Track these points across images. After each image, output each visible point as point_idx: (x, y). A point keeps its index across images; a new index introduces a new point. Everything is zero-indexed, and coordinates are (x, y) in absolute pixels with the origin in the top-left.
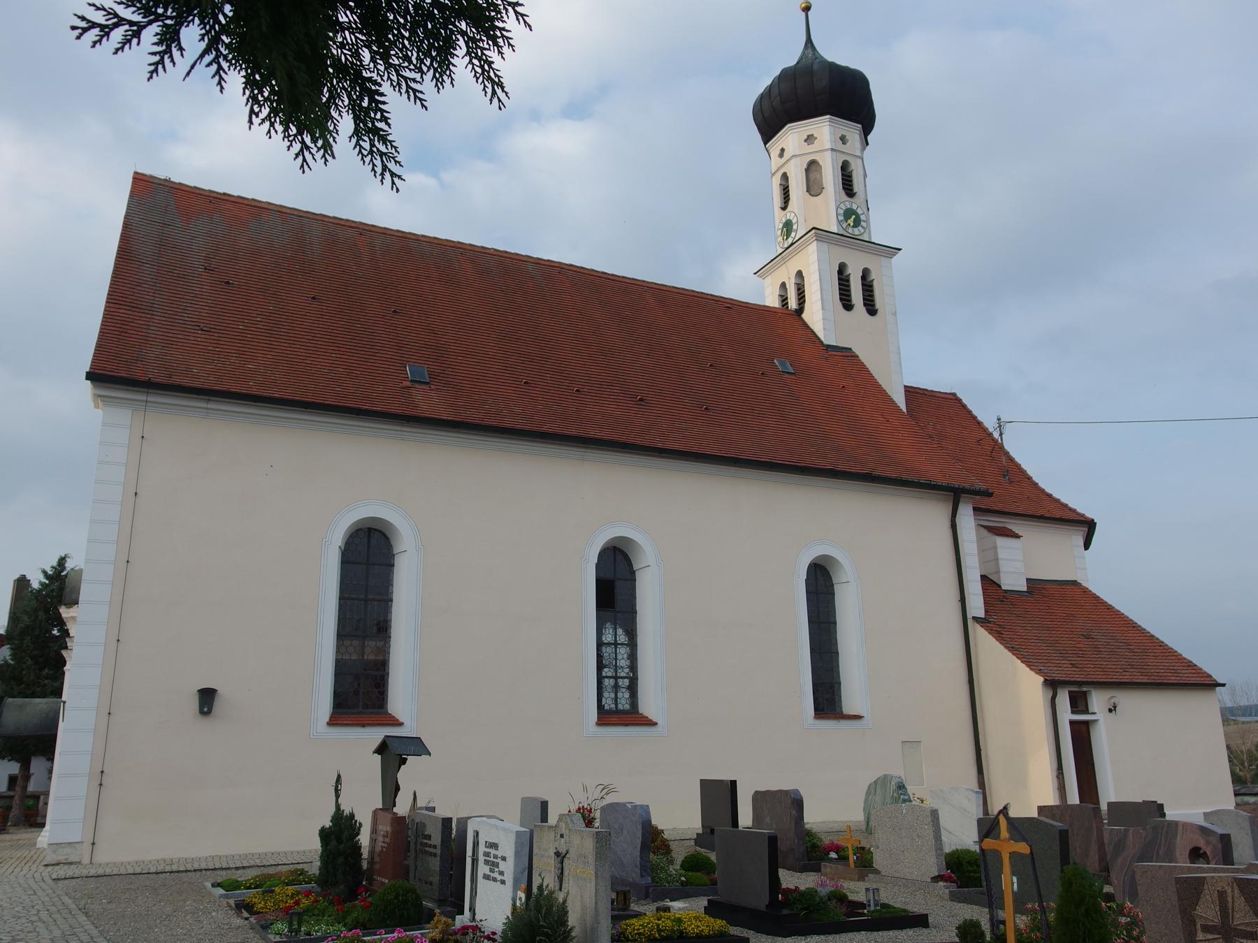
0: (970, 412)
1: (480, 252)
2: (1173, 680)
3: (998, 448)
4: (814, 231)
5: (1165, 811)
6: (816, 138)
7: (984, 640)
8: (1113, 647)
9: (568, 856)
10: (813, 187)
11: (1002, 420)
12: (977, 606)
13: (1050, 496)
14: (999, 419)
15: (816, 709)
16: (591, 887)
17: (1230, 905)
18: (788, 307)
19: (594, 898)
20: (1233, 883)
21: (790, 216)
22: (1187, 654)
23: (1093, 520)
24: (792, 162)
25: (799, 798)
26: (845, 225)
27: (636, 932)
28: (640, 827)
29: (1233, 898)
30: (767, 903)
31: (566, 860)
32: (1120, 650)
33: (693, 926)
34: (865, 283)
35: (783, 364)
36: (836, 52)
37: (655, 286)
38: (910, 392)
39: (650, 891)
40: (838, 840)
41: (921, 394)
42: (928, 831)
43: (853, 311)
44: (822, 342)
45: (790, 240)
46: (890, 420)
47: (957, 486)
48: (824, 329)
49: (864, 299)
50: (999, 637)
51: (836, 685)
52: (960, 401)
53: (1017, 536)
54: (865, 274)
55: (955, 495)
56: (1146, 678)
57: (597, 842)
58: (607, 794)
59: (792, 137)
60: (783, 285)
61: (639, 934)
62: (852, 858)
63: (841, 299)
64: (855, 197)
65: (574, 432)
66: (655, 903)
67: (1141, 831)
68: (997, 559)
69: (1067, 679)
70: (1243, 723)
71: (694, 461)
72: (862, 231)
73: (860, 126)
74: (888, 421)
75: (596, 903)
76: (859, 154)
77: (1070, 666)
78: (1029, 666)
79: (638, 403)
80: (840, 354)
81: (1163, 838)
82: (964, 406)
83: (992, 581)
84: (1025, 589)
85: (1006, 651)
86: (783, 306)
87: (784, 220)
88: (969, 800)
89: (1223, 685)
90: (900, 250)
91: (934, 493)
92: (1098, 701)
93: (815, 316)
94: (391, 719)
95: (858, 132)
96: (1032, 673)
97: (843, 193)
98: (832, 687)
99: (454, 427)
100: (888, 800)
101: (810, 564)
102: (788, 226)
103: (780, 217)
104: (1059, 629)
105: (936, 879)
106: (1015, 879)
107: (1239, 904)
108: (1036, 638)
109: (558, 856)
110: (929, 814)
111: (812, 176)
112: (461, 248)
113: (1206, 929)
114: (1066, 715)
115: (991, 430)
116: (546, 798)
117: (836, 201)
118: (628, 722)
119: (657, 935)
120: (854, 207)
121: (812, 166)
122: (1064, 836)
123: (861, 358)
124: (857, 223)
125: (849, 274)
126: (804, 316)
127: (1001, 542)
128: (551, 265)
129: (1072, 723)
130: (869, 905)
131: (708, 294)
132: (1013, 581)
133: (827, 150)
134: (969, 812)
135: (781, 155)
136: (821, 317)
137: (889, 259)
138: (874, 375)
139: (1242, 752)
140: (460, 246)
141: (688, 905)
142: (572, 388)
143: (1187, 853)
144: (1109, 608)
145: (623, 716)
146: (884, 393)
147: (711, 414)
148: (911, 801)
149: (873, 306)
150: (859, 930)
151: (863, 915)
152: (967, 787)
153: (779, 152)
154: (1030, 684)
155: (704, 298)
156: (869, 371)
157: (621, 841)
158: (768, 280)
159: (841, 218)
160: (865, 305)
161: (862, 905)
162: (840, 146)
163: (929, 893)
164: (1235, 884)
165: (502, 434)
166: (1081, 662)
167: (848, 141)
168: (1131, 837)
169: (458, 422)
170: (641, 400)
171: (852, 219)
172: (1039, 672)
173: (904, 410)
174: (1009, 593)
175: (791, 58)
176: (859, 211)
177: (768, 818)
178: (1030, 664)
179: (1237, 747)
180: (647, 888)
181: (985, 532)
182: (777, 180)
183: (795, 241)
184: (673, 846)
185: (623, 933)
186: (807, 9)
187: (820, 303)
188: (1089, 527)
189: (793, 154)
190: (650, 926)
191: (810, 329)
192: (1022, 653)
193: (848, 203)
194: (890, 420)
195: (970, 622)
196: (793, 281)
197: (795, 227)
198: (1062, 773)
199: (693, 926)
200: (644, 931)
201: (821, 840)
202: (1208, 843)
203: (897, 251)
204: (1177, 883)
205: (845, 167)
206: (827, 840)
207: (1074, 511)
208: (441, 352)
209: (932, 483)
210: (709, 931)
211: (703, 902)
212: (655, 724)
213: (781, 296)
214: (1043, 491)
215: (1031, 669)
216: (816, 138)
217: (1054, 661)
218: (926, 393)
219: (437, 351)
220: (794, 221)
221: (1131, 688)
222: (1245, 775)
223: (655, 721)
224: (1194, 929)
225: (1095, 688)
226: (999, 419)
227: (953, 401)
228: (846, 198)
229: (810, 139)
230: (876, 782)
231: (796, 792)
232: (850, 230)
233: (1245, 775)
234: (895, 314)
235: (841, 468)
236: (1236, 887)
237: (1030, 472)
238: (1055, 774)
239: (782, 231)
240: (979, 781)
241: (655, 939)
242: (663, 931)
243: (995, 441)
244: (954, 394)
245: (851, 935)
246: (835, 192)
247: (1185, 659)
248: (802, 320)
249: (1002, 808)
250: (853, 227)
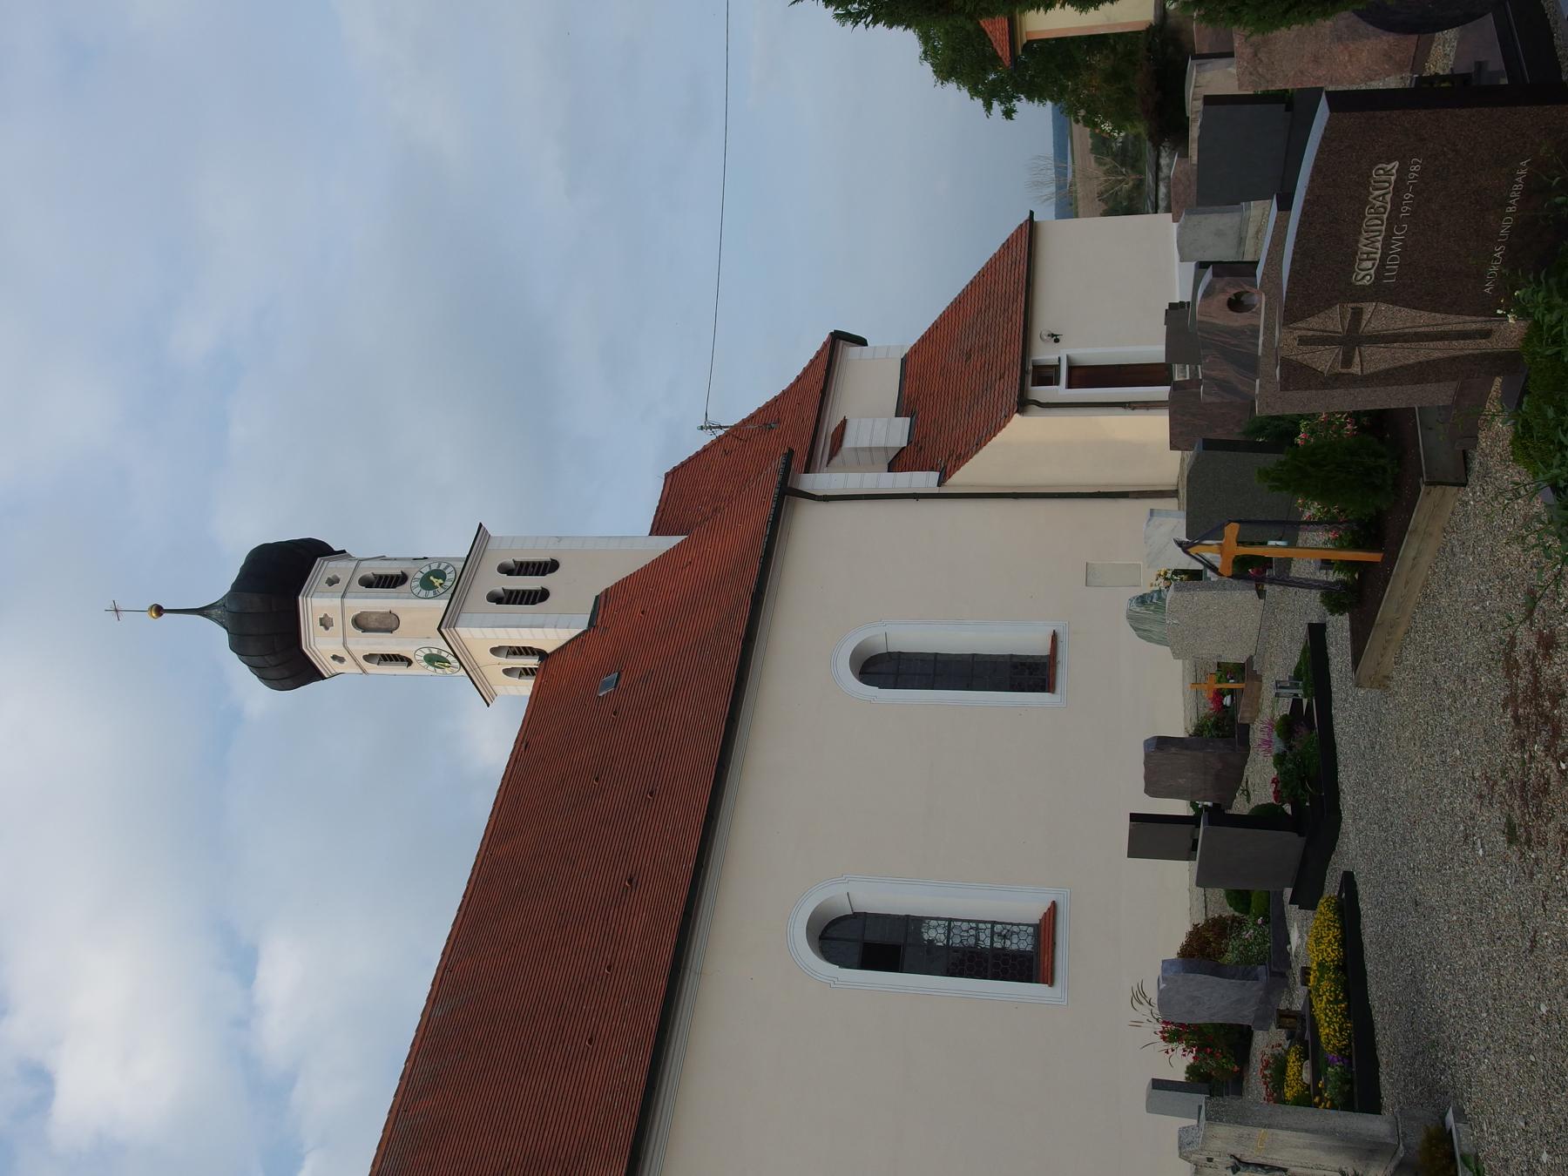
0: (690, 459)
1: (408, 1083)
2: (1023, 268)
3: (736, 432)
4: (443, 630)
5: (1178, 302)
6: (326, 615)
7: (966, 476)
8: (982, 329)
9: (1238, 1156)
10: (388, 624)
11: (703, 425)
12: (925, 480)
13: (799, 379)
14: (702, 428)
15: (1043, 690)
16: (1283, 1135)
17: (1318, 334)
18: (536, 669)
19: (1299, 1133)
20: (1289, 328)
21: (421, 655)
22: (995, 248)
23: (831, 334)
24: (351, 647)
25: (1155, 741)
26: (441, 590)
27: (1338, 1034)
28: (1191, 976)
29: (1309, 330)
30: (1296, 835)
31: (1245, 1159)
32: (986, 321)
33: (1329, 949)
34: (505, 599)
35: (606, 685)
36: (220, 581)
37: (487, 841)
38: (658, 528)
39: (1276, 970)
40: (1207, 695)
41: (662, 515)
43: (560, 562)
44: (584, 632)
45: (451, 659)
47: (777, 490)
48: (568, 628)
49: (537, 575)
50: (963, 458)
51: (1015, 660)
52: (675, 470)
53: (844, 422)
54: (506, 570)
55: (788, 494)
56: (1020, 296)
57: (1221, 1121)
58: (1145, 997)
59: (319, 644)
60: (507, 672)
61: (1341, 1030)
62: (1232, 684)
64: (407, 574)
65: (663, 983)
66: (1293, 965)
67: (1207, 361)
68: (870, 449)
69: (1017, 387)
70: (1074, 176)
71: (717, 822)
72: (451, 569)
73: (319, 559)
74: (690, 563)
75: (1307, 1131)
76: (353, 564)
77: (1002, 380)
78: (1000, 429)
79: (634, 886)
80: (601, 611)
81: (1216, 339)
82: (683, 465)
83: (895, 457)
84: (908, 419)
85: (981, 452)
86: (533, 674)
87: (425, 664)
88: (1161, 525)
89: (1032, 213)
90: (481, 525)
91: (783, 524)
92: (1044, 353)
93: (550, 638)
94: (1047, 918)
96: (1008, 425)
97: (399, 588)
98: (1015, 666)
100: (1158, 617)
101: (861, 680)
102: (432, 659)
103: (420, 669)
104: (958, 388)
105: (1261, 594)
106: (1271, 543)
107: (1315, 324)
108: (967, 415)
109: (1238, 1170)
110: (1180, 594)
111: (373, 625)
112: (398, 1111)
113: (1347, 362)
114: (1060, 392)
115: (714, 438)
116: (1148, 1081)
118: (1050, 943)
119: (1343, 1005)
120: (420, 576)
121: (360, 623)
122: (1209, 445)
124: (440, 574)
125: (503, 589)
126: (549, 650)
127: (849, 442)
128: (438, 983)
129: (1070, 386)
130: (1296, 695)
131: (506, 771)
132: (897, 433)
134: (1175, 527)
135: (341, 660)
136: (553, 630)
137: (491, 541)
138: (639, 568)
139: (1106, 181)
140: (395, 1112)
141: (1295, 924)
142: (605, 975)
143: (1235, 314)
144: (936, 327)
145: (1042, 946)
146: (655, 563)
147: (658, 788)
148: (1160, 591)
149: (546, 563)
150: (1330, 717)
151: (1309, 706)
152: (1144, 526)
153: (336, 662)
154: (1021, 429)
155: (511, 776)
157: (1209, 1000)
158: (499, 690)
159: (431, 593)
160: (543, 574)
161: (1296, 703)
162: (340, 587)
163: (1278, 604)
164: (1291, 325)
166: (998, 368)
167: (335, 576)
168: (1212, 373)
169: (632, 1152)
170: (630, 881)
171: (435, 580)
172: (1008, 418)
173: (683, 537)
174: (911, 439)
175: (221, 636)
176: (426, 570)
177: (1180, 780)
178: (998, 425)
179: (1101, 184)
180: (1273, 974)
181: (836, 460)
182: (372, 668)
183: (450, 651)
184: (1214, 913)
185: (1340, 1051)
186: (159, 610)
187: (534, 630)
188: (839, 339)
190: (1330, 1013)
191: (566, 644)
192: (984, 435)
193: (414, 584)
194: (690, 560)
195: (943, 490)
196: (503, 660)
197: (435, 651)
198: (1129, 403)
199: (1329, 949)
200: (1337, 1022)
201: (1207, 717)
202: (1223, 291)
203: (482, 528)
204: (1287, 389)
205: (367, 583)
206: (1208, 708)
207: (819, 354)
208: (534, 1162)
209: (771, 519)
210: (1335, 927)
211: (1293, 912)
212: (1054, 903)
213: (520, 676)
214: (792, 386)
215: (1004, 426)
216: (326, 615)
217: (996, 399)
218: (662, 508)
219: (532, 1168)
220: (428, 652)
221: (1032, 313)
222: (1133, 180)
223: (1050, 904)
224: (1347, 376)
225: (1029, 356)
226: (702, 428)
227: (673, 477)
229: (325, 623)
230: (1136, 629)
231: (1147, 743)
232: (448, 584)
233: (1133, 180)
234: (560, 539)
235: (742, 631)
236: (1295, 325)
237: (769, 398)
238: (1129, 411)
239: (438, 667)
240: (1137, 498)
241: (1348, 1008)
242: (1337, 996)
243: (727, 434)
244: (667, 475)
245: (1337, 729)
246: (397, 598)
247: (999, 251)
248: (554, 652)
249: (1180, 549)
250: (444, 581)
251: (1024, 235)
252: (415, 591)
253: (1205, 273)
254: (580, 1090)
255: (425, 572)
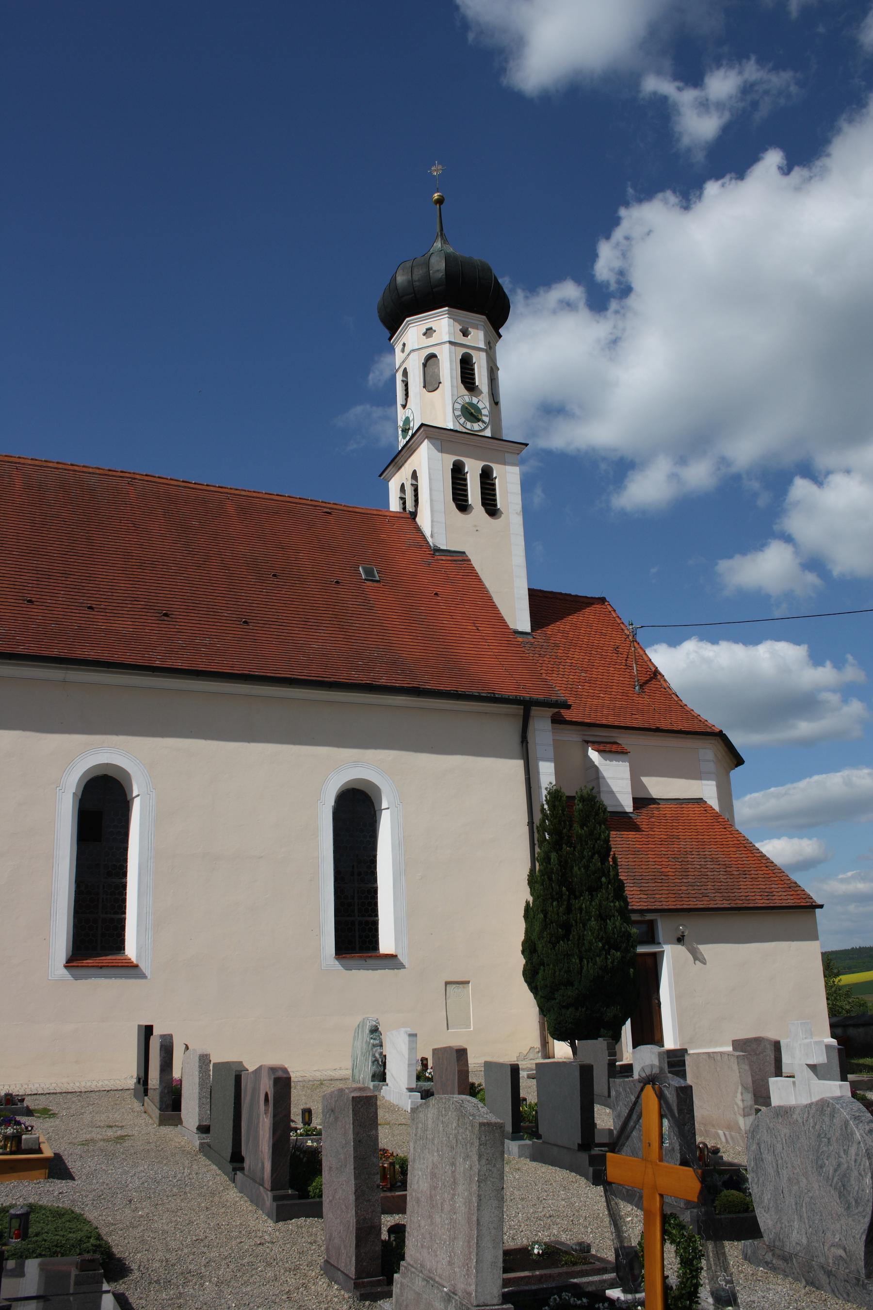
10: (431, 383)
42: (771, 1056)
46: (480, 628)
60: (403, 486)
63: (454, 499)
79: (161, 619)
80: (449, 558)
89: (821, 906)
95: (482, 323)
99: (330, 687)
117: (452, 395)
123: (473, 562)
133: (444, 343)
135: (403, 351)
156: (480, 579)
162: (461, 339)
165: (330, 688)
189: (412, 349)
203: (523, 446)
209: (497, 696)
216: (435, 331)
220: (411, 419)
228: (466, 392)
229: (429, 332)
251: (799, 901)
252: (459, 400)
253: (837, 1080)
254: (376, 627)
255: (478, 405)
